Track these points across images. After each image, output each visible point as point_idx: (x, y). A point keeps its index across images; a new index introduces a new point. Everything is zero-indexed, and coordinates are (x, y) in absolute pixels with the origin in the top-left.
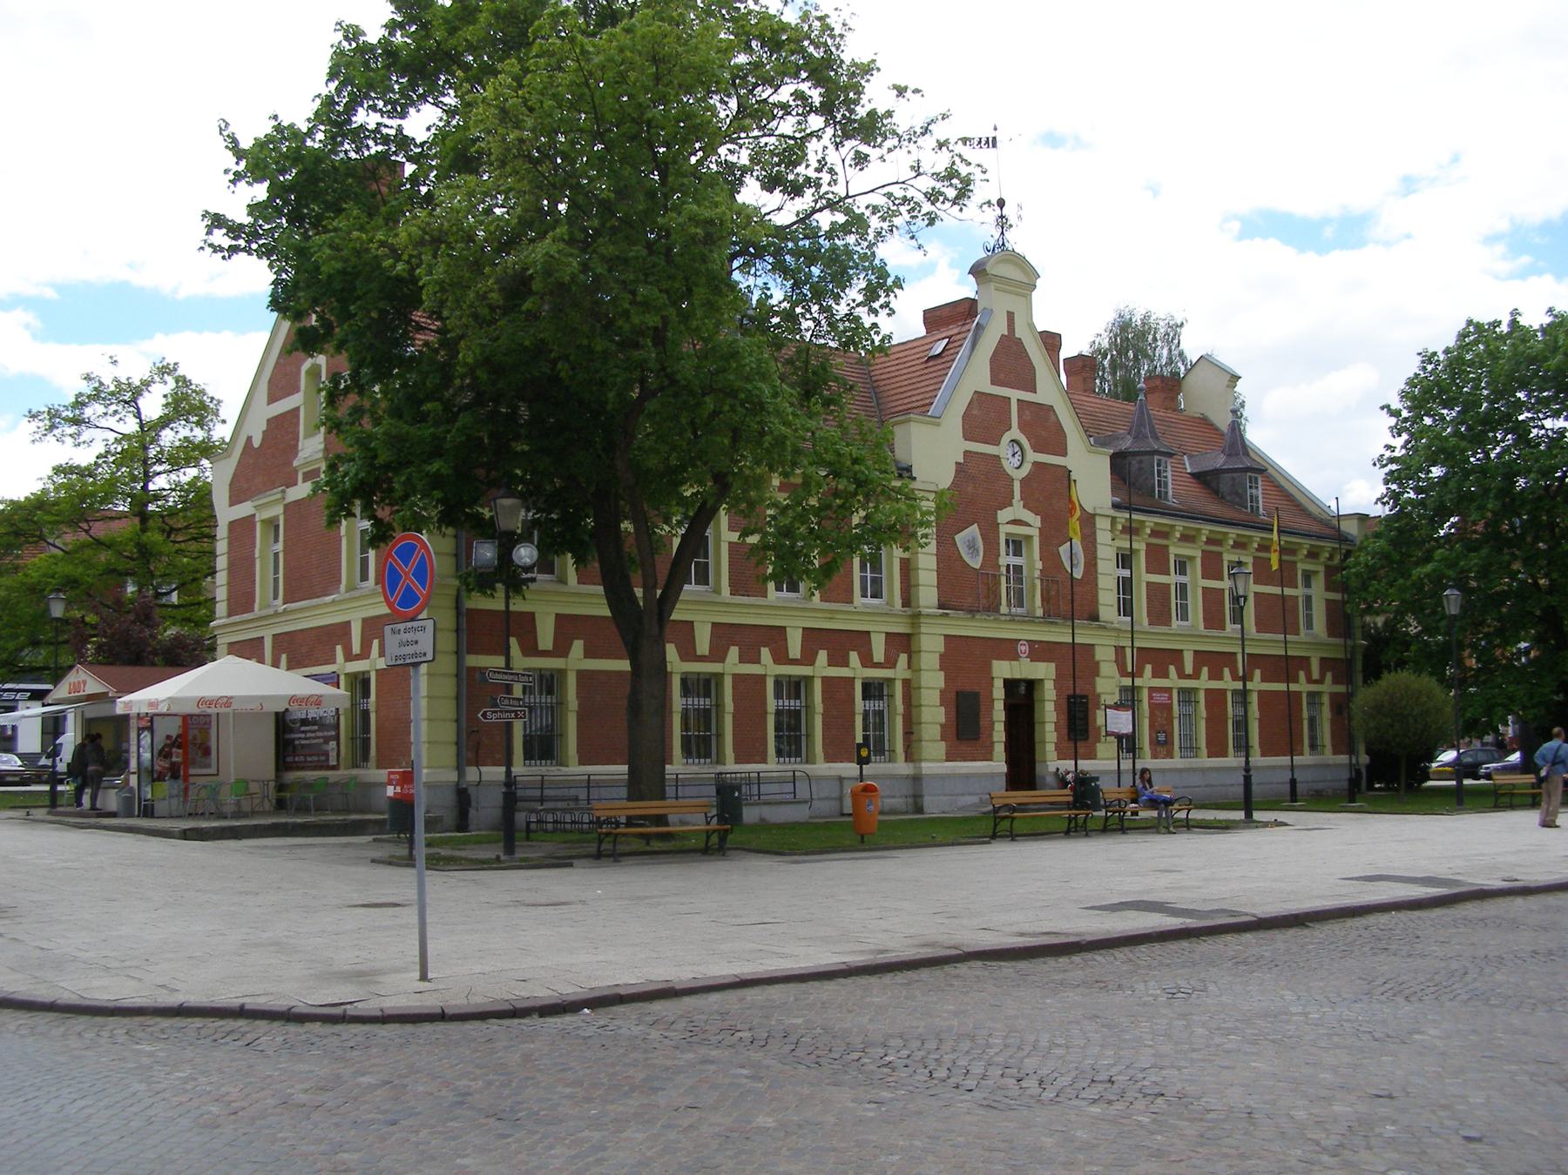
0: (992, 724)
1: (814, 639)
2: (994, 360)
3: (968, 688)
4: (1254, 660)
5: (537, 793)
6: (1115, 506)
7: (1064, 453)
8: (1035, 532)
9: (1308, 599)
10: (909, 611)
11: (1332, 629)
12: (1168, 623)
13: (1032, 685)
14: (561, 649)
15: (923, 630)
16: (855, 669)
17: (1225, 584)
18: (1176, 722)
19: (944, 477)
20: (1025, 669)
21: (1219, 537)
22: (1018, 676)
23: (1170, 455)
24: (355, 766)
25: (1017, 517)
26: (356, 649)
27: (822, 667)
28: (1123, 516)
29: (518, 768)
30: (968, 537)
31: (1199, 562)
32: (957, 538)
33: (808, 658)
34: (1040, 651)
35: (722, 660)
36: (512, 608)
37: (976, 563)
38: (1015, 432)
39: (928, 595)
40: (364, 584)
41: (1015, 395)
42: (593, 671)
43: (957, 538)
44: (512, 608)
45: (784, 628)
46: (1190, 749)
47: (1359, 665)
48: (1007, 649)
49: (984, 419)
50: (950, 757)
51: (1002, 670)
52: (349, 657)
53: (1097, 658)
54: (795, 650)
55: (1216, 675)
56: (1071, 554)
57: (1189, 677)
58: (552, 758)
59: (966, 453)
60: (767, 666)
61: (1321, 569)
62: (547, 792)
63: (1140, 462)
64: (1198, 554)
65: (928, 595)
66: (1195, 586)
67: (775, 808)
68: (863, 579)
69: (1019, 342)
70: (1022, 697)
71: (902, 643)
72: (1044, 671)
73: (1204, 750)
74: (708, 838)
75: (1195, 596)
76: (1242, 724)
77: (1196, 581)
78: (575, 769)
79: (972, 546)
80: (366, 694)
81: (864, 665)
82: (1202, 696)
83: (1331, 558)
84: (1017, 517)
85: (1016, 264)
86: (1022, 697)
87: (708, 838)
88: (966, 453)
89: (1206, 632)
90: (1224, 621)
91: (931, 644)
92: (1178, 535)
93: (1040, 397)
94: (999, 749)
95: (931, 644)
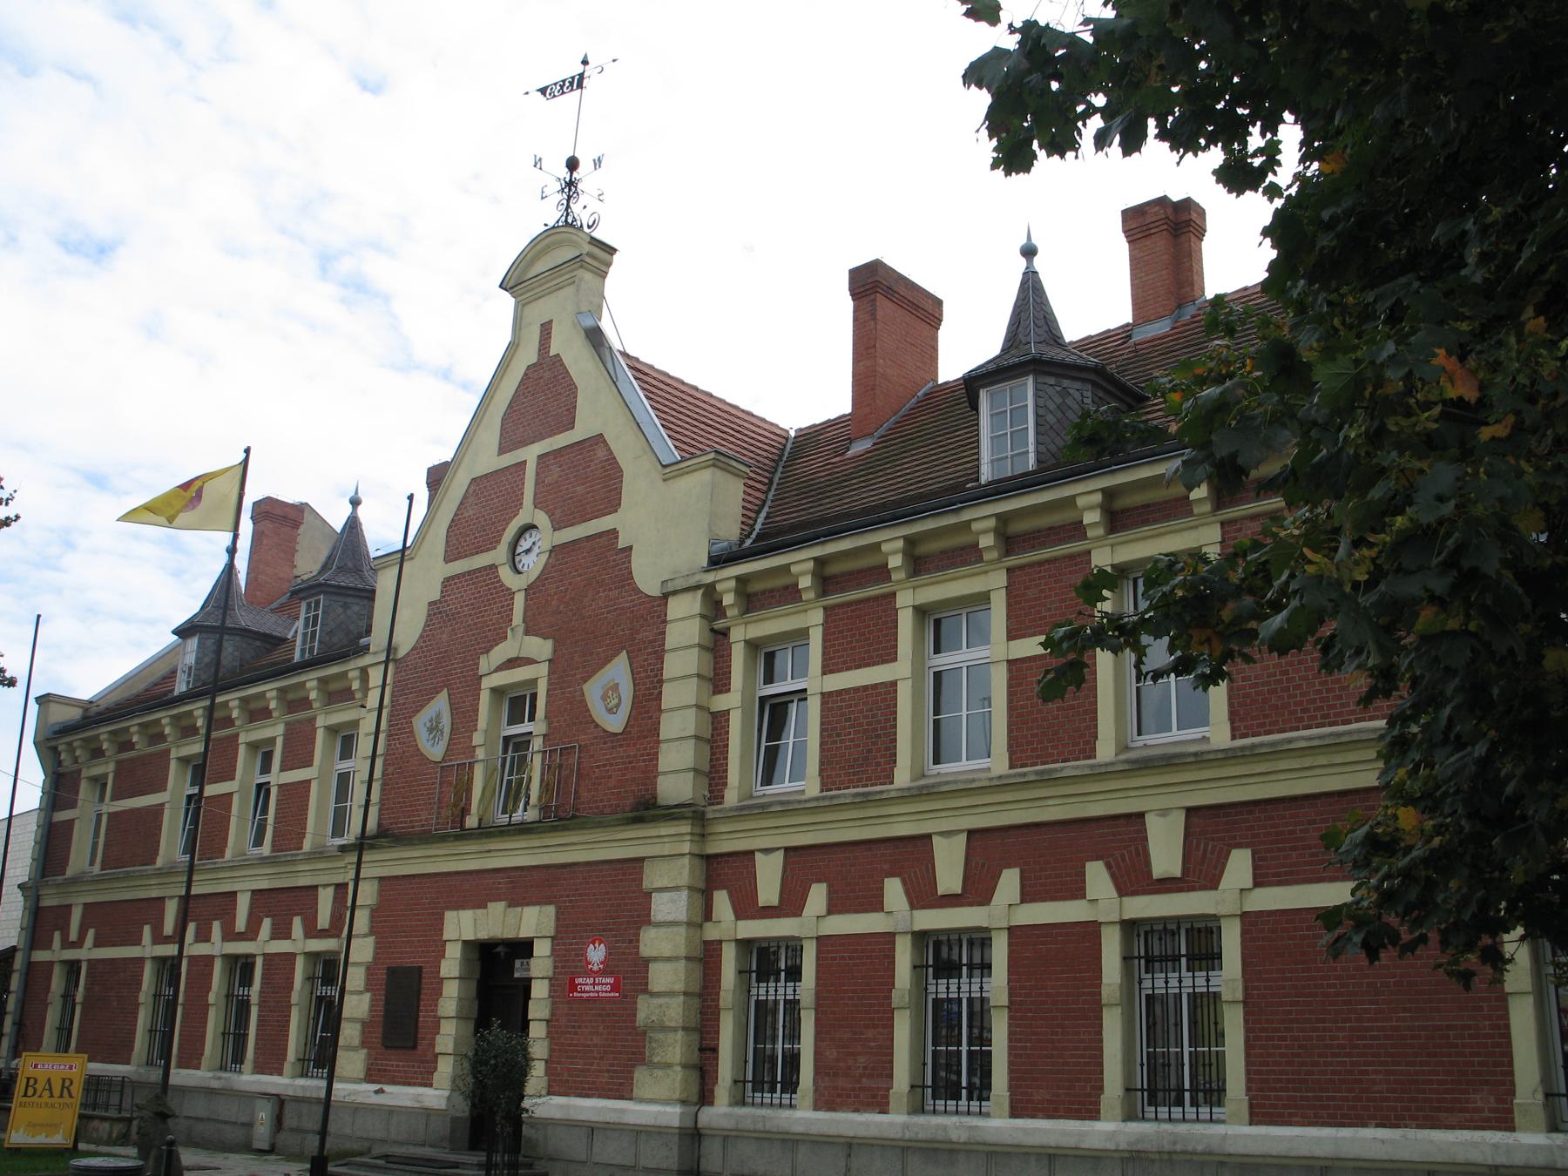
1: (803, 864)
3: (409, 962)
4: (803, 864)
14: (791, 903)
24: (223, 1068)
26: (73, 936)
27: (817, 918)
29: (352, 1087)
33: (977, 889)
34: (520, 887)
35: (1212, 883)
37: (435, 751)
40: (257, 851)
45: (1141, 815)
52: (159, 939)
53: (647, 884)
54: (949, 877)
60: (1100, 898)
70: (497, 965)
72: (534, 922)
76: (328, 1014)
77: (812, 678)
79: (434, 728)
80: (247, 980)
82: (1231, 942)
86: (497, 965)
94: (445, 1068)
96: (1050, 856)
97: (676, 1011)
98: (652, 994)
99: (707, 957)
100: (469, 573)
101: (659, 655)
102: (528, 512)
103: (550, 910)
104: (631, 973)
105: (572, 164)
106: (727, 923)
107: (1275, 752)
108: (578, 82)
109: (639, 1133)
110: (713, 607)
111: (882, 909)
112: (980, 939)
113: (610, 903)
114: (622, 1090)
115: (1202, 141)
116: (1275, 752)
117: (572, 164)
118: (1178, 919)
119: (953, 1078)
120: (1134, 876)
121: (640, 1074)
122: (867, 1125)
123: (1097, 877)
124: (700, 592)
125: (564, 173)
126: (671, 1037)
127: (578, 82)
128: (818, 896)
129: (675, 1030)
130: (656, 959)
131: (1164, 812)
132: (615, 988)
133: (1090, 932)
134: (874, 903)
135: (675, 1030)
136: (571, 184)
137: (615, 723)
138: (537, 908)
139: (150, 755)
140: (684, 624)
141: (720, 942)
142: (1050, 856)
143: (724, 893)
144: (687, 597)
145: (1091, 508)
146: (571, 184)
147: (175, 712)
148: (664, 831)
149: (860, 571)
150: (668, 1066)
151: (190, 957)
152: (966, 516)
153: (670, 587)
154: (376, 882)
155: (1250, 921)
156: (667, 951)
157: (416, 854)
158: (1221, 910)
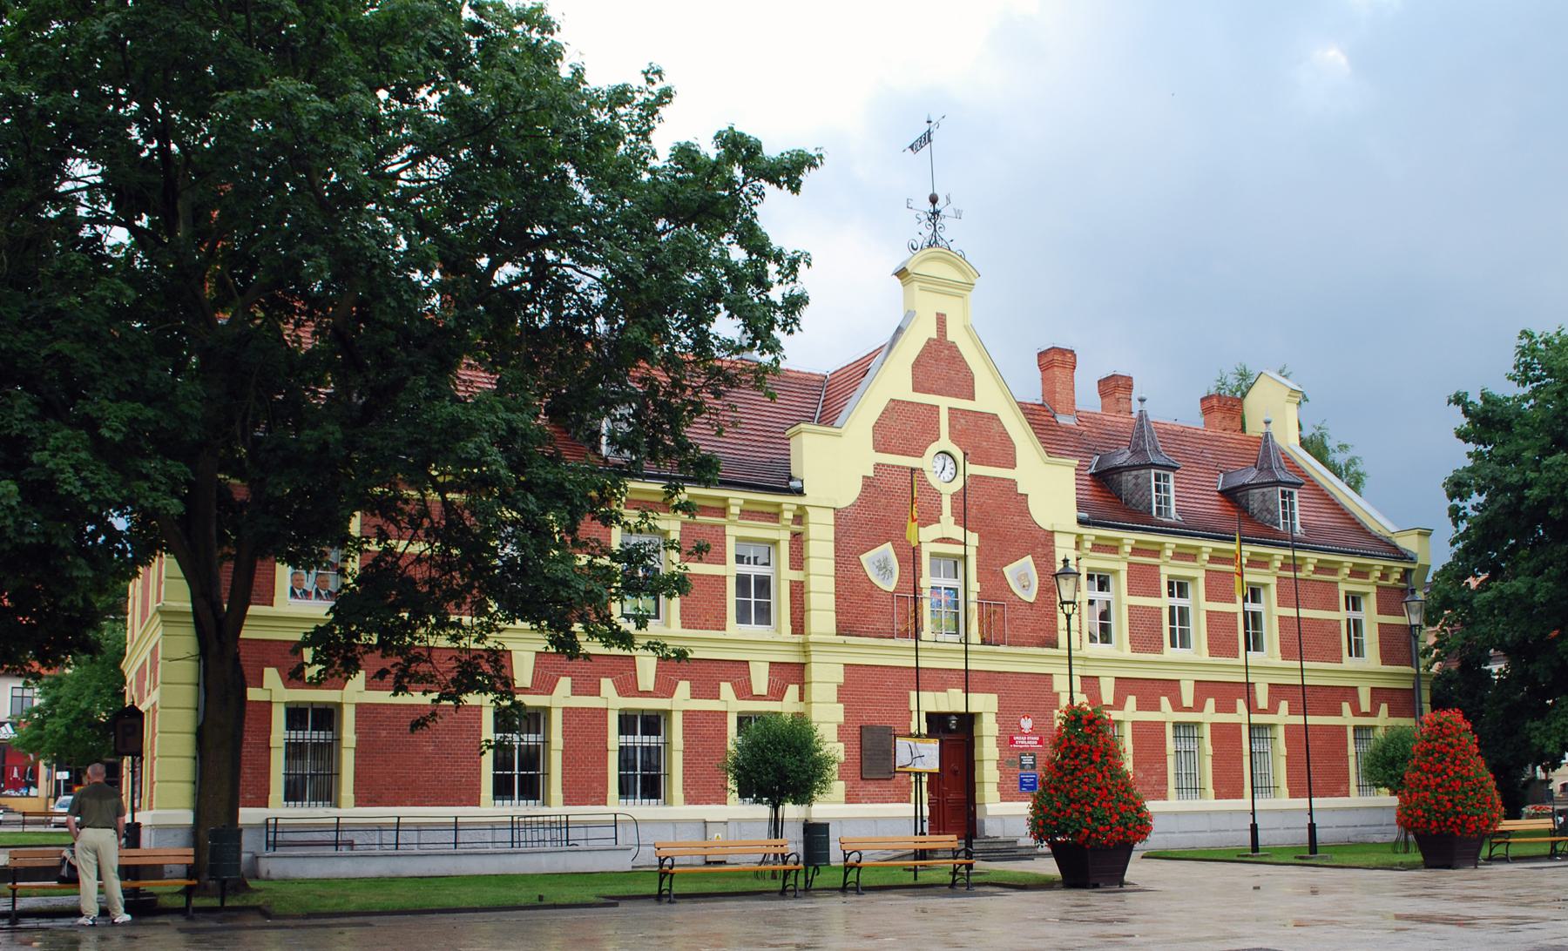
2: (917, 365)
4: (1276, 691)
5: (331, 836)
6: (1081, 522)
7: (1013, 466)
9: (1356, 626)
10: (798, 638)
11: (1387, 656)
12: (1158, 648)
13: (968, 721)
15: (813, 658)
16: (1240, 715)
17: (1237, 608)
18: (1171, 761)
19: (848, 494)
20: (951, 701)
21: (1193, 552)
22: (944, 708)
23: (1174, 469)
25: (939, 535)
28: (1092, 533)
30: (880, 565)
31: (1273, 590)
32: (863, 558)
33: (1199, 706)
34: (968, 681)
35: (670, 694)
38: (945, 443)
39: (822, 618)
41: (944, 403)
43: (863, 558)
46: (1191, 788)
47: (1426, 696)
48: (919, 678)
49: (902, 429)
54: (1188, 700)
55: (1225, 706)
56: (1022, 576)
57: (1366, 714)
58: (658, 797)
59: (878, 466)
61: (1373, 590)
62: (280, 837)
63: (1137, 477)
64: (1201, 575)
65: (822, 618)
66: (1197, 609)
67: (464, 859)
68: (1172, 631)
69: (953, 347)
70: (955, 733)
71: (792, 674)
73: (1210, 790)
74: (846, 874)
75: (1270, 626)
77: (1199, 604)
78: (348, 810)
79: (883, 567)
81: (740, 696)
82: (1207, 732)
83: (1384, 576)
84: (939, 535)
87: (846, 874)
88: (878, 466)
90: (724, 618)
91: (826, 675)
92: (1169, 553)
93: (978, 405)
95: (826, 675)
105: (934, 200)
108: (927, 138)
115: (144, 222)
117: (934, 200)
119: (583, 789)
120: (744, 691)
123: (726, 689)
125: (929, 207)
127: (927, 138)
128: (1131, 701)
132: (1040, 742)
134: (1157, 708)
136: (936, 213)
137: (890, 585)
146: (936, 213)
155: (567, 712)
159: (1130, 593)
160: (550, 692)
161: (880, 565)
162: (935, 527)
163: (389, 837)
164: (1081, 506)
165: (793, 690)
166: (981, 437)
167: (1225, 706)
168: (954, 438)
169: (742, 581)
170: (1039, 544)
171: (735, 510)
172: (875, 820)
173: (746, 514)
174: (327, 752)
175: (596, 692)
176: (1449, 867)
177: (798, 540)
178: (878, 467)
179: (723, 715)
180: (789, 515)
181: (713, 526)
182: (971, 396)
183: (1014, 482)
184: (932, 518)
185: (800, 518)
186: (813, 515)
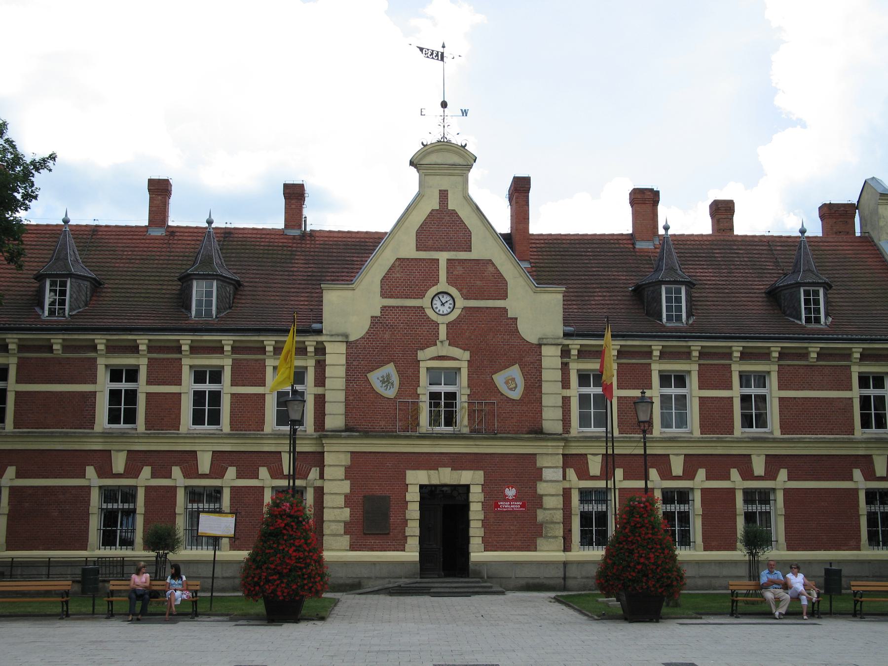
0: (405, 522)
2: (419, 233)
8: (464, 366)
19: (358, 328)
28: (575, 344)
30: (384, 380)
31: (695, 377)
34: (458, 462)
36: (648, 452)
41: (443, 257)
42: (50, 487)
44: (648, 452)
50: (353, 548)
51: (417, 478)
56: (510, 381)
69: (454, 213)
77: (693, 391)
79: (386, 381)
81: (867, 478)
82: (697, 497)
85: (448, 151)
89: (465, 477)
93: (473, 255)
96: (718, 466)
97: (559, 516)
98: (545, 509)
99: (566, 494)
100: (402, 307)
101: (539, 369)
102: (443, 284)
103: (481, 473)
104: (537, 501)
106: (574, 481)
107: (800, 441)
109: (735, 563)
110: (565, 352)
111: (170, 477)
112: (218, 491)
113: (526, 472)
114: (531, 546)
116: (800, 441)
118: (756, 489)
120: (747, 474)
121: (539, 541)
122: (378, 557)
123: (857, 474)
124: (560, 347)
126: (557, 526)
129: (559, 523)
130: (546, 495)
131: (759, 455)
133: (732, 492)
135: (559, 523)
137: (516, 395)
138: (472, 472)
139: (63, 358)
140: (551, 358)
141: (570, 489)
142: (718, 466)
143: (92, 468)
144: (553, 348)
145: (737, 351)
147: (66, 337)
148: (550, 444)
149: (759, 353)
150: (556, 537)
151: (619, 489)
152: (690, 344)
153: (545, 341)
154: (349, 455)
155: (148, 489)
156: (553, 492)
157: (365, 442)
158: (777, 487)
159: (780, 388)
160: (137, 477)
161: (384, 380)
162: (433, 348)
163: (44, 571)
164: (566, 322)
165: (314, 473)
166: (479, 279)
167: (161, 471)
168: (450, 281)
169: (745, 399)
170: (528, 356)
171: (656, 353)
172: (374, 563)
173: (664, 355)
174: (110, 518)
175: (169, 476)
176: (651, 621)
177: (321, 366)
178: (384, 308)
179: (856, 491)
180: (311, 349)
181: (257, 360)
182: (469, 249)
183: (504, 310)
184: (432, 341)
185: (320, 350)
186: (329, 348)
